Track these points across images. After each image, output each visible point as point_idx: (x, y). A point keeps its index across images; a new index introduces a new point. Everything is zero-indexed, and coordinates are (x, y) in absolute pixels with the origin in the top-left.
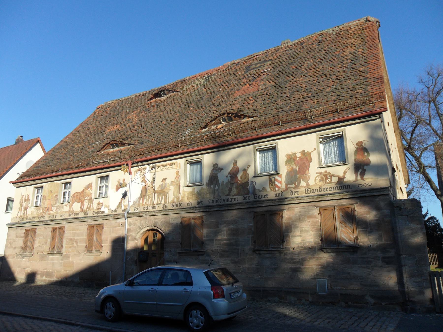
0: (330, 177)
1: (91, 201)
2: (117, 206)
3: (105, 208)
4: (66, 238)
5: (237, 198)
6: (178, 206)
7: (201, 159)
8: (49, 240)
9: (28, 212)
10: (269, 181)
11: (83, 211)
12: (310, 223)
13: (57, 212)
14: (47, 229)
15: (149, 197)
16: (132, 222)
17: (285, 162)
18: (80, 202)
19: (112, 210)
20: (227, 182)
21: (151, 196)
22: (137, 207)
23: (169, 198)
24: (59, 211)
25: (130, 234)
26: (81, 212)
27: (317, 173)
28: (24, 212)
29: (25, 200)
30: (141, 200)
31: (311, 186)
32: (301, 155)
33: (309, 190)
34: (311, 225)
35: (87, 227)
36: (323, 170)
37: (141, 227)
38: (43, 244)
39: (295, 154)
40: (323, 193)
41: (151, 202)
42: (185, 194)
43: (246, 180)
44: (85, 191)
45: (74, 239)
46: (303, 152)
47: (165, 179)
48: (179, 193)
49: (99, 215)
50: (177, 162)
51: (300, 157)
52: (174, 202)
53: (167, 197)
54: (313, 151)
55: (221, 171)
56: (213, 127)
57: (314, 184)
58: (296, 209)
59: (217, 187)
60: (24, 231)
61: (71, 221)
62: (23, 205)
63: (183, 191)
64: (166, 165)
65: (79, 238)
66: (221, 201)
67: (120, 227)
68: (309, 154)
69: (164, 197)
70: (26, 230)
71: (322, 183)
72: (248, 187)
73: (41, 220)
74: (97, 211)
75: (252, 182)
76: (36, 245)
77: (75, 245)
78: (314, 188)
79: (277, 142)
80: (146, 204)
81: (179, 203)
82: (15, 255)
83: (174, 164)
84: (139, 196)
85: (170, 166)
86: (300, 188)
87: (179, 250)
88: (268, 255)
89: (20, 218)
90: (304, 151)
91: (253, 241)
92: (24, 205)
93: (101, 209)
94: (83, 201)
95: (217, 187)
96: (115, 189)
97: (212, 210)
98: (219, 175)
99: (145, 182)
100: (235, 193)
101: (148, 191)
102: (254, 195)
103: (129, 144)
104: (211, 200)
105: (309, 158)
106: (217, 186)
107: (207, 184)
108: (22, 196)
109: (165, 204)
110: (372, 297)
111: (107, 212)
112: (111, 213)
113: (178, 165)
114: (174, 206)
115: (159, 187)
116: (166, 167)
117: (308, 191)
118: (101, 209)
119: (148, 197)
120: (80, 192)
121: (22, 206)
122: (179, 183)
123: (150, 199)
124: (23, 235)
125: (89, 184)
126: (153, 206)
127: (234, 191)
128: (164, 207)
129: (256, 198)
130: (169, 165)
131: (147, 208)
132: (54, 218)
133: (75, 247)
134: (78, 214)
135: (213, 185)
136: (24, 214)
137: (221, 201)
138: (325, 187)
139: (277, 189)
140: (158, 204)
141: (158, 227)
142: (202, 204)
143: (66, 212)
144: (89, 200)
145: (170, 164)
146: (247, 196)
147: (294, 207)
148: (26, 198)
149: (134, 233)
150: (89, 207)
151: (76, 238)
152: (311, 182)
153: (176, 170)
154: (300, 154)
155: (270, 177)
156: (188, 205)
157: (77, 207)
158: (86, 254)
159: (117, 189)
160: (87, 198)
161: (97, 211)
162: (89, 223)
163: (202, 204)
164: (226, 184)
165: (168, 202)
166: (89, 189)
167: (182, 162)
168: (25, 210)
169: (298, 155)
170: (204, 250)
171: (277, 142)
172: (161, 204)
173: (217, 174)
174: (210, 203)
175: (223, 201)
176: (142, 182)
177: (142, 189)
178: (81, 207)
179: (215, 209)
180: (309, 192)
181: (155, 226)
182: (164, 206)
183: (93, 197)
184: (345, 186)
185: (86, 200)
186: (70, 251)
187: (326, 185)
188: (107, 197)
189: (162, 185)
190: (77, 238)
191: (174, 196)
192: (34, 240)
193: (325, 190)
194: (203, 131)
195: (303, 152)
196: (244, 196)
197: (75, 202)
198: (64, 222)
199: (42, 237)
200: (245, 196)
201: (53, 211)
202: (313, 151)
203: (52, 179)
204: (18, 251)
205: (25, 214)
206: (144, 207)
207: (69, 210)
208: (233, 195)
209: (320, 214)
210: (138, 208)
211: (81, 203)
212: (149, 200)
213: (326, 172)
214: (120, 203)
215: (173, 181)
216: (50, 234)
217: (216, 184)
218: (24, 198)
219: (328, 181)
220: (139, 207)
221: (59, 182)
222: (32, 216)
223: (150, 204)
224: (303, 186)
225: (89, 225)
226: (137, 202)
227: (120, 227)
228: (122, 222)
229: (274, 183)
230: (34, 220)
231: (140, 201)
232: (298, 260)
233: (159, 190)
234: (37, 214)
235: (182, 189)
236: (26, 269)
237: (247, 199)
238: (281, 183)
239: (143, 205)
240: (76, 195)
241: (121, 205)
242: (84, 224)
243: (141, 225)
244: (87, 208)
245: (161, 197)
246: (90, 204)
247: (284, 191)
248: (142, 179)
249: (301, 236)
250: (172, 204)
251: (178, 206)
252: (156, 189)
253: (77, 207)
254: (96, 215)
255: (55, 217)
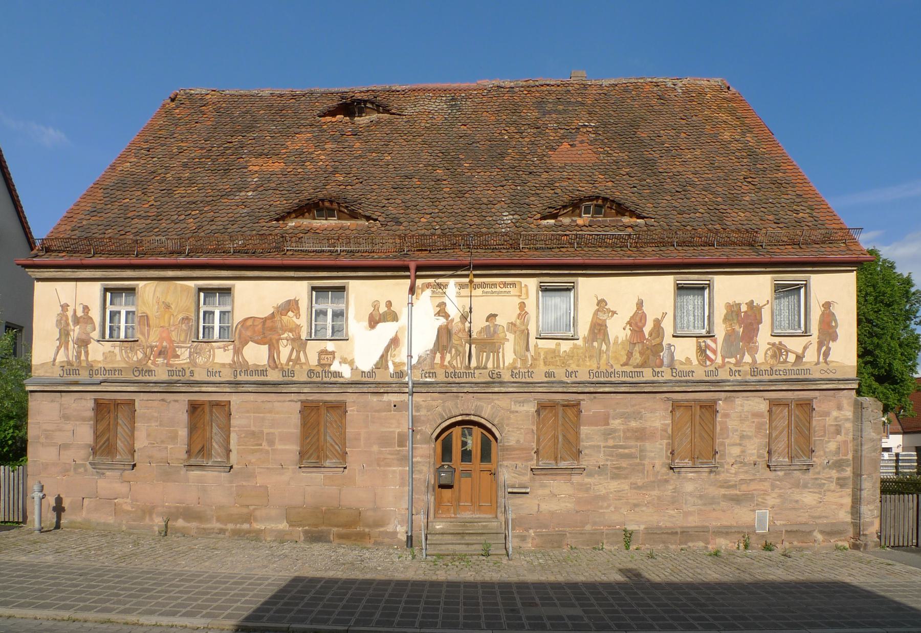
0: (785, 353)
1: (299, 344)
2: (375, 362)
3: (343, 365)
4: (236, 429)
5: (642, 372)
6: (527, 376)
7: (572, 284)
8: (183, 433)
9: (90, 352)
10: (697, 346)
11: (277, 367)
12: (754, 425)
13: (196, 363)
14: (170, 402)
15: (457, 350)
16: (422, 403)
17: (723, 317)
18: (264, 344)
19: (362, 372)
20: (624, 339)
21: (461, 349)
22: (427, 369)
23: (503, 357)
24: (200, 360)
25: (419, 428)
26: (273, 369)
27: (769, 344)
28: (79, 353)
29: (77, 321)
30: (438, 355)
31: (760, 364)
32: (747, 308)
33: (755, 370)
34: (756, 428)
35: (298, 406)
36: (777, 340)
37: (444, 414)
38: (162, 442)
39: (740, 304)
40: (774, 377)
41: (461, 364)
42: (539, 353)
43: (657, 341)
44: (277, 318)
45: (262, 432)
46: (750, 304)
47: (495, 316)
48: (527, 349)
49: (325, 380)
50: (521, 283)
51: (745, 312)
52: (515, 368)
53: (500, 355)
54: (765, 305)
55: (612, 316)
56: (566, 220)
57: (764, 361)
58: (737, 400)
59: (604, 347)
60: (91, 404)
61: (250, 389)
62: (71, 333)
63: (536, 346)
64: (494, 285)
65: (276, 431)
66: (613, 375)
67: (393, 412)
68: (759, 309)
69: (492, 354)
70: (95, 400)
71: (771, 361)
72: (662, 354)
73: (140, 378)
74: (319, 369)
75: (669, 344)
76: (141, 441)
77: (265, 446)
78: (763, 368)
79: (712, 278)
80: (450, 365)
81: (528, 372)
82: (69, 464)
83: (514, 284)
84: (431, 346)
85: (504, 289)
86: (743, 366)
87: (533, 464)
88: (691, 474)
89: (67, 367)
90: (752, 302)
91: (669, 452)
92: (76, 332)
93: (330, 365)
94: (274, 341)
95: (604, 347)
96: (366, 323)
97: (601, 390)
98: (609, 323)
99: (447, 316)
100: (638, 361)
101: (454, 337)
102: (671, 369)
103: (368, 218)
104: (594, 372)
105: (758, 318)
106: (605, 344)
107: (584, 338)
108: (65, 307)
109: (497, 371)
110: (822, 532)
111: (347, 373)
112: (358, 378)
113: (524, 290)
114: (517, 376)
115: (481, 332)
116: (494, 290)
117: (754, 371)
118: (332, 367)
119: (453, 351)
120: (262, 318)
121: (68, 334)
122: (527, 329)
123: (459, 355)
124: (91, 414)
125: (289, 302)
126: (467, 371)
127: (636, 359)
128: (495, 376)
129: (674, 374)
130: (502, 286)
131: (455, 375)
132: (187, 377)
133: (267, 452)
134: (264, 372)
135: (597, 341)
136: (78, 356)
137: (613, 375)
138: (778, 368)
139: (708, 363)
140: (477, 368)
141: (486, 417)
142: (576, 377)
143: (223, 365)
144: (293, 340)
145: (505, 285)
146: (660, 370)
147: (734, 397)
148: (80, 313)
149: (428, 426)
150: (293, 357)
151: (266, 431)
152: (760, 358)
153: (518, 301)
154: (746, 306)
155: (699, 341)
156: (547, 375)
157: (256, 354)
158: (303, 470)
159: (373, 322)
160: (285, 335)
161: (319, 369)
162: (303, 397)
163: (576, 377)
164: (623, 342)
165: (501, 366)
166: (290, 314)
167: (532, 284)
168: (79, 347)
169: (744, 308)
170: (582, 465)
171: (712, 278)
172: (485, 368)
173: (605, 320)
174: (592, 377)
175: (616, 375)
176: (438, 314)
177: (438, 331)
178: (271, 356)
179: (607, 390)
180: (756, 373)
181: (478, 414)
182: (492, 373)
183: (304, 336)
184: (364, 372)
185: (285, 342)
186: (253, 460)
187: (779, 365)
188: (348, 340)
189: (488, 327)
190: (272, 431)
191: (515, 355)
192: (133, 429)
193: (778, 373)
194: (545, 222)
195: (750, 304)
196: (655, 369)
197: (250, 342)
198: (228, 390)
199: (157, 424)
200: (657, 370)
201: (181, 357)
202: (765, 305)
203: (170, 273)
204: (80, 455)
205: (83, 357)
206: (446, 372)
207: (233, 361)
208: (635, 364)
209: (770, 411)
210: (429, 373)
211: (269, 345)
212: (458, 357)
213: (780, 343)
214: (382, 356)
215: (512, 323)
216: (184, 417)
217: (604, 340)
218: (70, 313)
219: (782, 360)
220: (432, 371)
221: (192, 284)
222: (108, 366)
223: (459, 366)
224: (748, 363)
225: (302, 402)
226: (428, 360)
227: (393, 412)
228: (396, 401)
229: (705, 351)
230: (116, 377)
231: (434, 358)
232: (733, 483)
233: (480, 338)
234: (127, 363)
235: (532, 341)
236: (116, 501)
237: (659, 375)
238: (714, 352)
239: (442, 365)
240: (249, 323)
241: (387, 361)
242: (288, 399)
243: (444, 411)
244: (289, 360)
245: (485, 354)
246: (298, 352)
247: (719, 367)
248: (438, 309)
249: (740, 445)
250: (512, 372)
251: (527, 376)
252: (474, 335)
253: (256, 354)
254: (319, 379)
255: (188, 374)
